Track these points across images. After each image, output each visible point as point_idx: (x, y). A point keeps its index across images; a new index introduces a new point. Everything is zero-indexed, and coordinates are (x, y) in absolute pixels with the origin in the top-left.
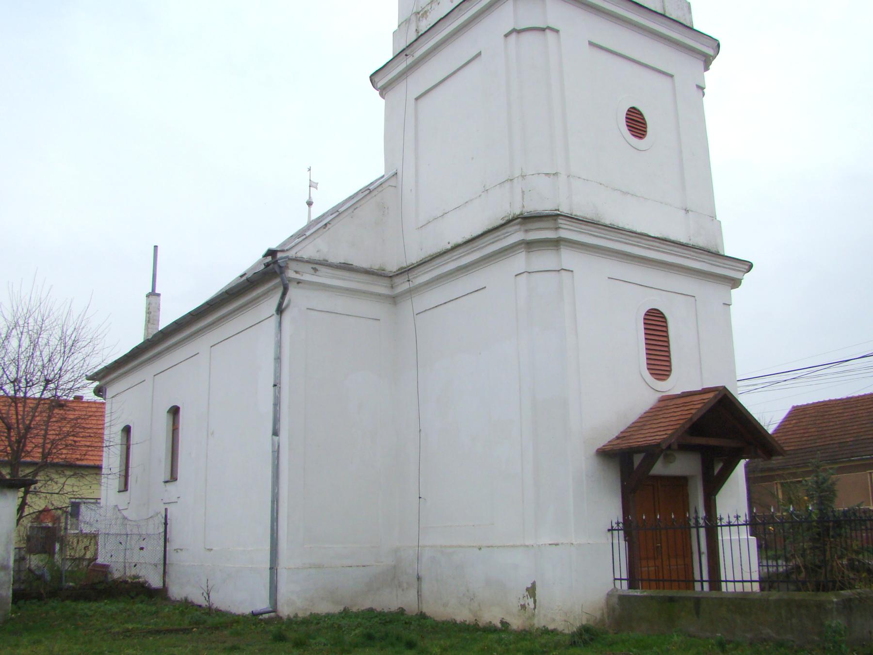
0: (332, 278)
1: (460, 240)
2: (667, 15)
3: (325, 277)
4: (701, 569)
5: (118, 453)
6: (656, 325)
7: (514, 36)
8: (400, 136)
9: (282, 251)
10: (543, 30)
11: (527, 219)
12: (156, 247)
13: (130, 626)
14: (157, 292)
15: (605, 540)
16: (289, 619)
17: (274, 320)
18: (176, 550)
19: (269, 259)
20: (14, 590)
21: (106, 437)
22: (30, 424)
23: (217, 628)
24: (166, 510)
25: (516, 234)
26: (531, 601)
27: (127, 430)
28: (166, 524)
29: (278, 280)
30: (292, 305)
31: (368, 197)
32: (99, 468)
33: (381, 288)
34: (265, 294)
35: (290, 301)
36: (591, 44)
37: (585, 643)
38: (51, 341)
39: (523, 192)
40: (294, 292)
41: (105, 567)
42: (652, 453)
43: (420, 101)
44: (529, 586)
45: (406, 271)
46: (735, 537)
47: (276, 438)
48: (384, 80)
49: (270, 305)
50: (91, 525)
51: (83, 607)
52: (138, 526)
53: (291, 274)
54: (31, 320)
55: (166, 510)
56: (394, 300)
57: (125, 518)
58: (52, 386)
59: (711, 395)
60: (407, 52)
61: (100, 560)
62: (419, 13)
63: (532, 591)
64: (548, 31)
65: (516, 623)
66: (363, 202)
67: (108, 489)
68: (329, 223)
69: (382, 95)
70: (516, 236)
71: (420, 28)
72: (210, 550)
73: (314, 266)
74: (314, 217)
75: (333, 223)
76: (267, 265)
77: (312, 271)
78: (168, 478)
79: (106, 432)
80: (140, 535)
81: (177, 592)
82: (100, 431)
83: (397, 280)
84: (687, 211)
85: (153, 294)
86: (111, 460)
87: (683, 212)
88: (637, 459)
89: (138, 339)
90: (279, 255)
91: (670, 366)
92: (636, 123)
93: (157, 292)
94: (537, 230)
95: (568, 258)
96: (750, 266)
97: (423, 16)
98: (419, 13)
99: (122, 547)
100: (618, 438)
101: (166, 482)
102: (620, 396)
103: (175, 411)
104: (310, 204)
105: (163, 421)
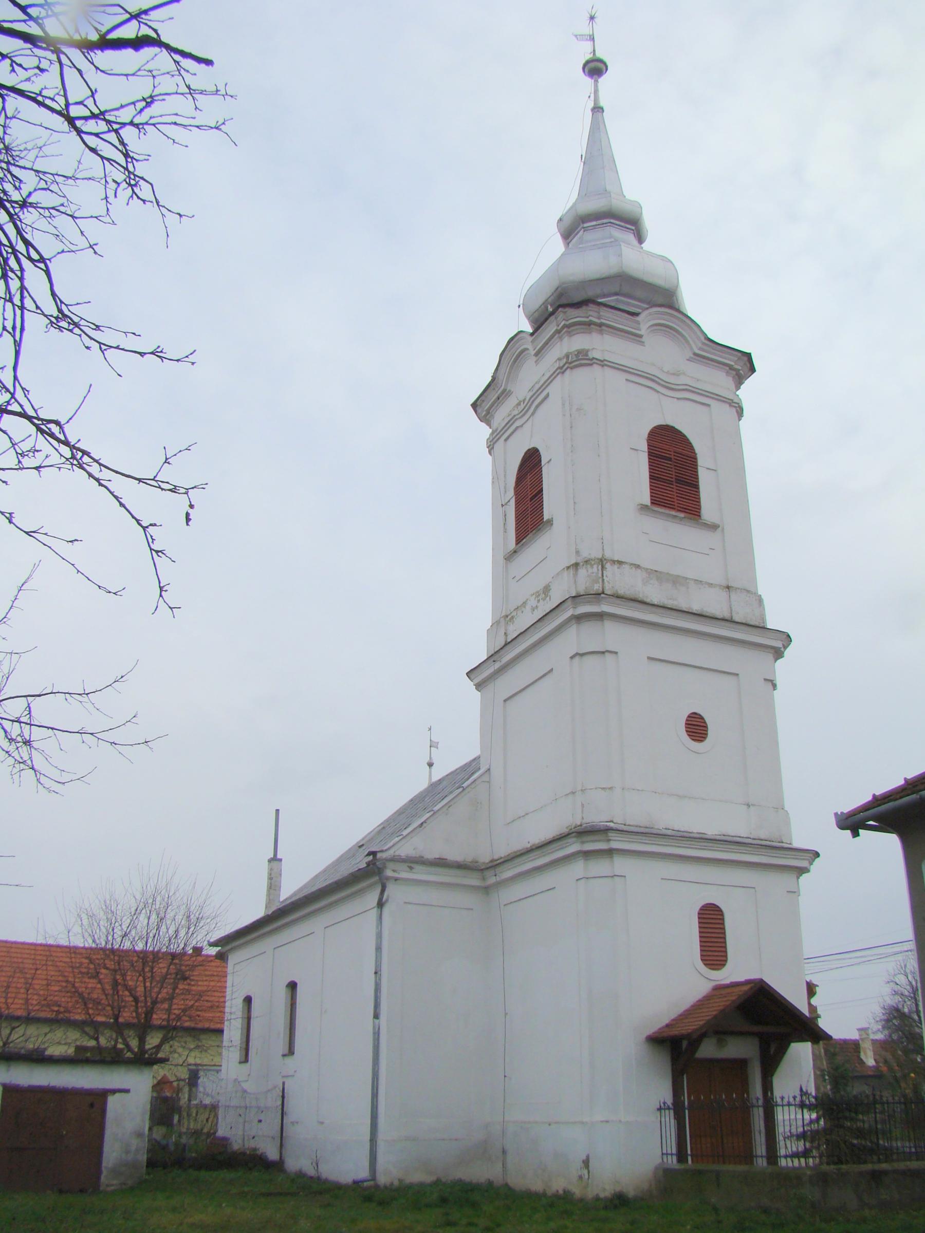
2: (737, 618)
3: (420, 873)
4: (760, 1148)
5: (240, 1026)
6: (711, 921)
7: (577, 658)
8: (493, 726)
9: (382, 851)
10: (603, 653)
11: (584, 832)
12: (277, 811)
13: (246, 1189)
14: (279, 856)
15: (653, 1119)
16: (386, 1187)
17: (374, 913)
18: (292, 1123)
19: (371, 857)
20: (148, 1159)
21: (227, 1010)
22: (157, 998)
23: (321, 1193)
24: (284, 1083)
26: (586, 1172)
27: (248, 1000)
28: (283, 1097)
31: (463, 794)
32: (221, 1031)
33: (473, 880)
34: (361, 891)
35: (388, 896)
37: (616, 1207)
38: (175, 915)
39: (583, 805)
40: (391, 889)
41: (225, 1139)
42: (695, 1040)
44: (584, 1158)
45: (495, 865)
46: (799, 1116)
47: (377, 1021)
48: (483, 676)
49: (372, 898)
50: (212, 1097)
51: (204, 1174)
52: (257, 1099)
53: (389, 873)
54: (159, 899)
55: (284, 1083)
57: (245, 1091)
58: (177, 961)
59: (746, 988)
61: (220, 1133)
62: (507, 616)
63: (586, 1163)
65: (577, 1192)
67: (230, 1057)
68: (425, 822)
70: (574, 847)
72: (322, 1123)
74: (435, 778)
75: (428, 822)
76: (368, 864)
78: (286, 1051)
79: (227, 1004)
80: (259, 1107)
81: (293, 1164)
82: (222, 1000)
83: (488, 873)
84: (748, 805)
85: (275, 859)
86: (233, 1032)
87: (745, 807)
88: (685, 1044)
89: (259, 912)
90: (379, 855)
91: (726, 956)
92: (696, 727)
93: (279, 856)
94: (591, 840)
95: (620, 864)
96: (817, 855)
98: (507, 616)
99: (241, 1120)
100: (667, 1026)
101: (284, 1055)
102: (677, 984)
103: (293, 986)
104: (430, 765)
105: (282, 993)
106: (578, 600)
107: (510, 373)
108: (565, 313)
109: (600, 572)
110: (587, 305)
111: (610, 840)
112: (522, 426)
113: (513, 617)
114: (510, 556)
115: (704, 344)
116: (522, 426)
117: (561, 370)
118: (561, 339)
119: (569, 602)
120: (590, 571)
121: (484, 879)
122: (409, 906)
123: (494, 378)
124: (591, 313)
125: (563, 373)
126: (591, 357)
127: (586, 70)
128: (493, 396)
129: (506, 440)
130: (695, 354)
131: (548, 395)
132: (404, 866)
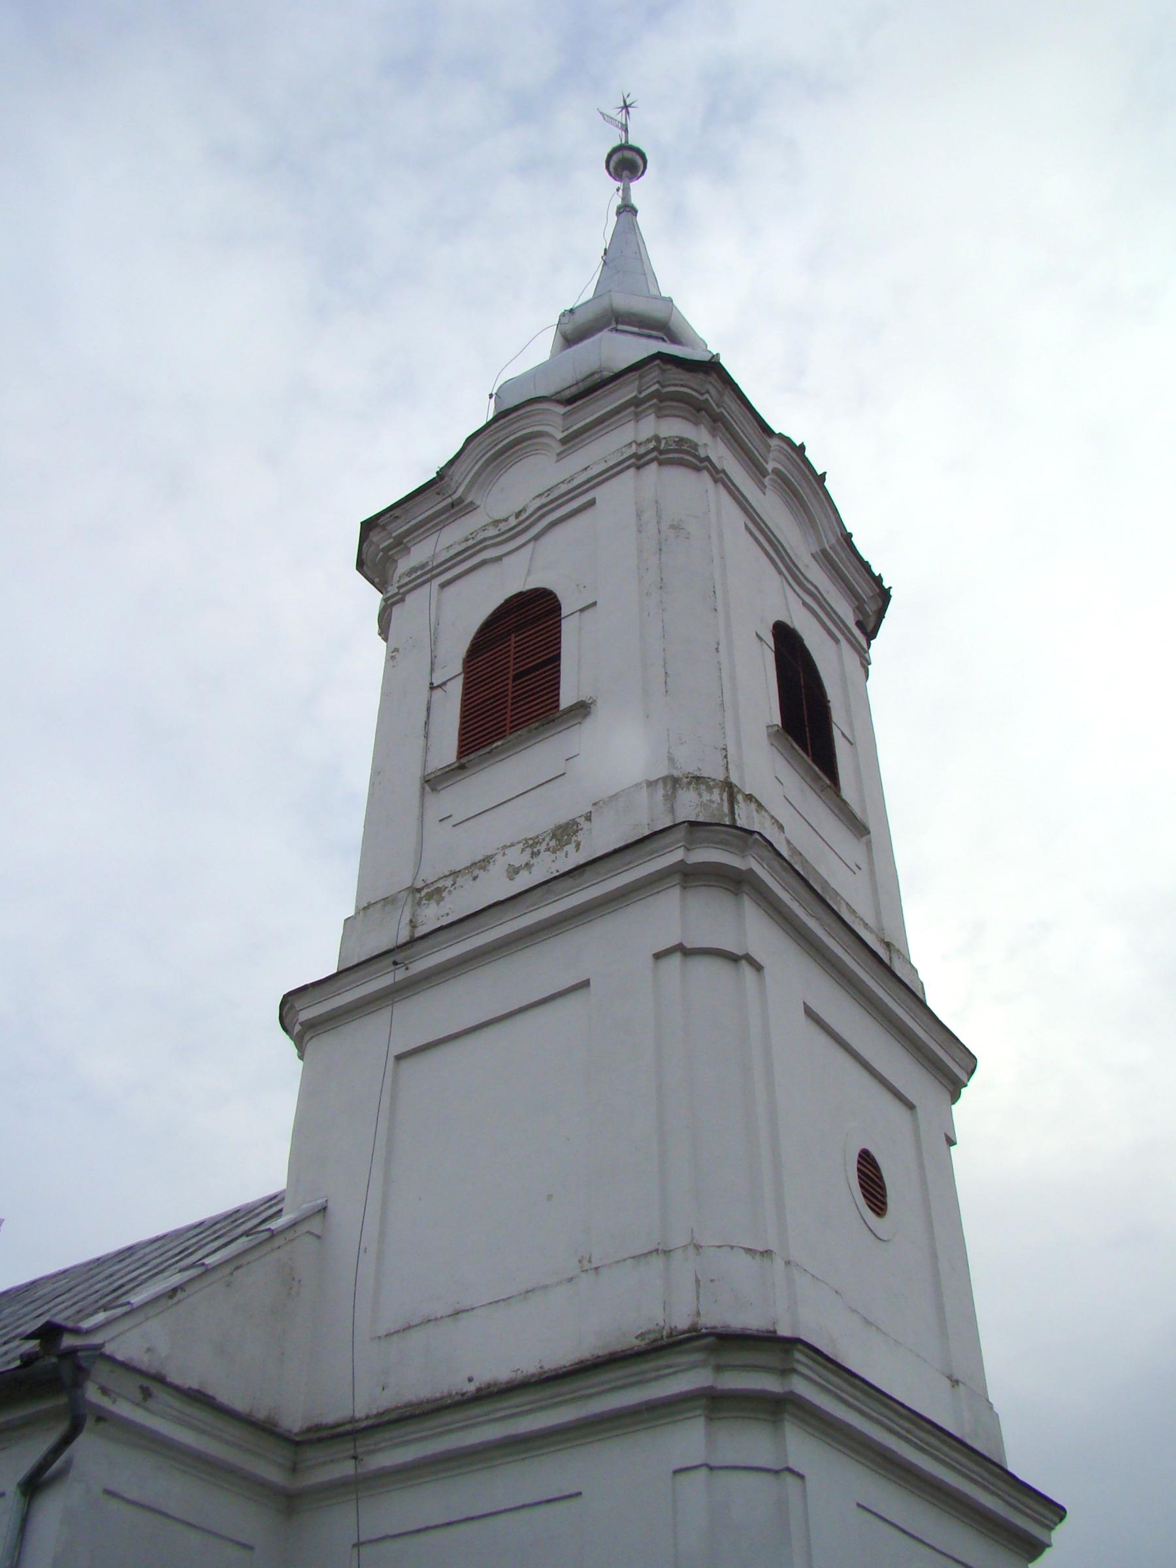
0: (179, 1421)
1: (504, 1374)
11: (728, 1343)
25: (691, 1375)
29: (63, 1400)
30: (73, 1473)
31: (266, 1248)
35: (69, 1463)
36: (809, 1013)
39: (697, 1281)
40: (89, 1449)
43: (405, 1064)
48: (306, 1015)
56: (290, 1503)
60: (399, 957)
62: (419, 890)
64: (743, 962)
66: (250, 1257)
69: (300, 1043)
71: (420, 919)
73: (147, 1383)
75: (190, 1290)
76: (28, 1360)
77: (139, 1396)
90: (68, 1341)
95: (800, 1447)
97: (429, 896)
106: (701, 833)
107: (478, 474)
108: (663, 371)
109: (726, 804)
110: (707, 373)
111: (794, 1371)
112: (499, 559)
113: (439, 891)
114: (433, 782)
115: (838, 540)
116: (499, 559)
117: (638, 462)
118: (638, 417)
119: (681, 833)
120: (706, 797)
121: (294, 1469)
122: (114, 1504)
123: (441, 474)
124: (710, 387)
125: (638, 468)
126: (703, 455)
127: (615, 158)
128: (432, 505)
129: (443, 586)
130: (824, 551)
131: (592, 503)
132: (131, 1385)
